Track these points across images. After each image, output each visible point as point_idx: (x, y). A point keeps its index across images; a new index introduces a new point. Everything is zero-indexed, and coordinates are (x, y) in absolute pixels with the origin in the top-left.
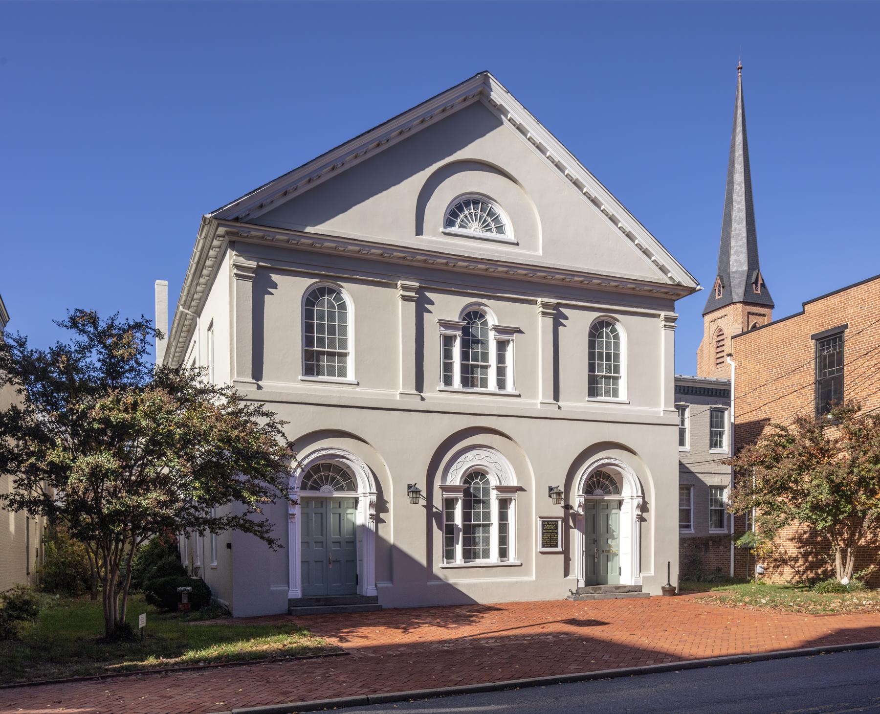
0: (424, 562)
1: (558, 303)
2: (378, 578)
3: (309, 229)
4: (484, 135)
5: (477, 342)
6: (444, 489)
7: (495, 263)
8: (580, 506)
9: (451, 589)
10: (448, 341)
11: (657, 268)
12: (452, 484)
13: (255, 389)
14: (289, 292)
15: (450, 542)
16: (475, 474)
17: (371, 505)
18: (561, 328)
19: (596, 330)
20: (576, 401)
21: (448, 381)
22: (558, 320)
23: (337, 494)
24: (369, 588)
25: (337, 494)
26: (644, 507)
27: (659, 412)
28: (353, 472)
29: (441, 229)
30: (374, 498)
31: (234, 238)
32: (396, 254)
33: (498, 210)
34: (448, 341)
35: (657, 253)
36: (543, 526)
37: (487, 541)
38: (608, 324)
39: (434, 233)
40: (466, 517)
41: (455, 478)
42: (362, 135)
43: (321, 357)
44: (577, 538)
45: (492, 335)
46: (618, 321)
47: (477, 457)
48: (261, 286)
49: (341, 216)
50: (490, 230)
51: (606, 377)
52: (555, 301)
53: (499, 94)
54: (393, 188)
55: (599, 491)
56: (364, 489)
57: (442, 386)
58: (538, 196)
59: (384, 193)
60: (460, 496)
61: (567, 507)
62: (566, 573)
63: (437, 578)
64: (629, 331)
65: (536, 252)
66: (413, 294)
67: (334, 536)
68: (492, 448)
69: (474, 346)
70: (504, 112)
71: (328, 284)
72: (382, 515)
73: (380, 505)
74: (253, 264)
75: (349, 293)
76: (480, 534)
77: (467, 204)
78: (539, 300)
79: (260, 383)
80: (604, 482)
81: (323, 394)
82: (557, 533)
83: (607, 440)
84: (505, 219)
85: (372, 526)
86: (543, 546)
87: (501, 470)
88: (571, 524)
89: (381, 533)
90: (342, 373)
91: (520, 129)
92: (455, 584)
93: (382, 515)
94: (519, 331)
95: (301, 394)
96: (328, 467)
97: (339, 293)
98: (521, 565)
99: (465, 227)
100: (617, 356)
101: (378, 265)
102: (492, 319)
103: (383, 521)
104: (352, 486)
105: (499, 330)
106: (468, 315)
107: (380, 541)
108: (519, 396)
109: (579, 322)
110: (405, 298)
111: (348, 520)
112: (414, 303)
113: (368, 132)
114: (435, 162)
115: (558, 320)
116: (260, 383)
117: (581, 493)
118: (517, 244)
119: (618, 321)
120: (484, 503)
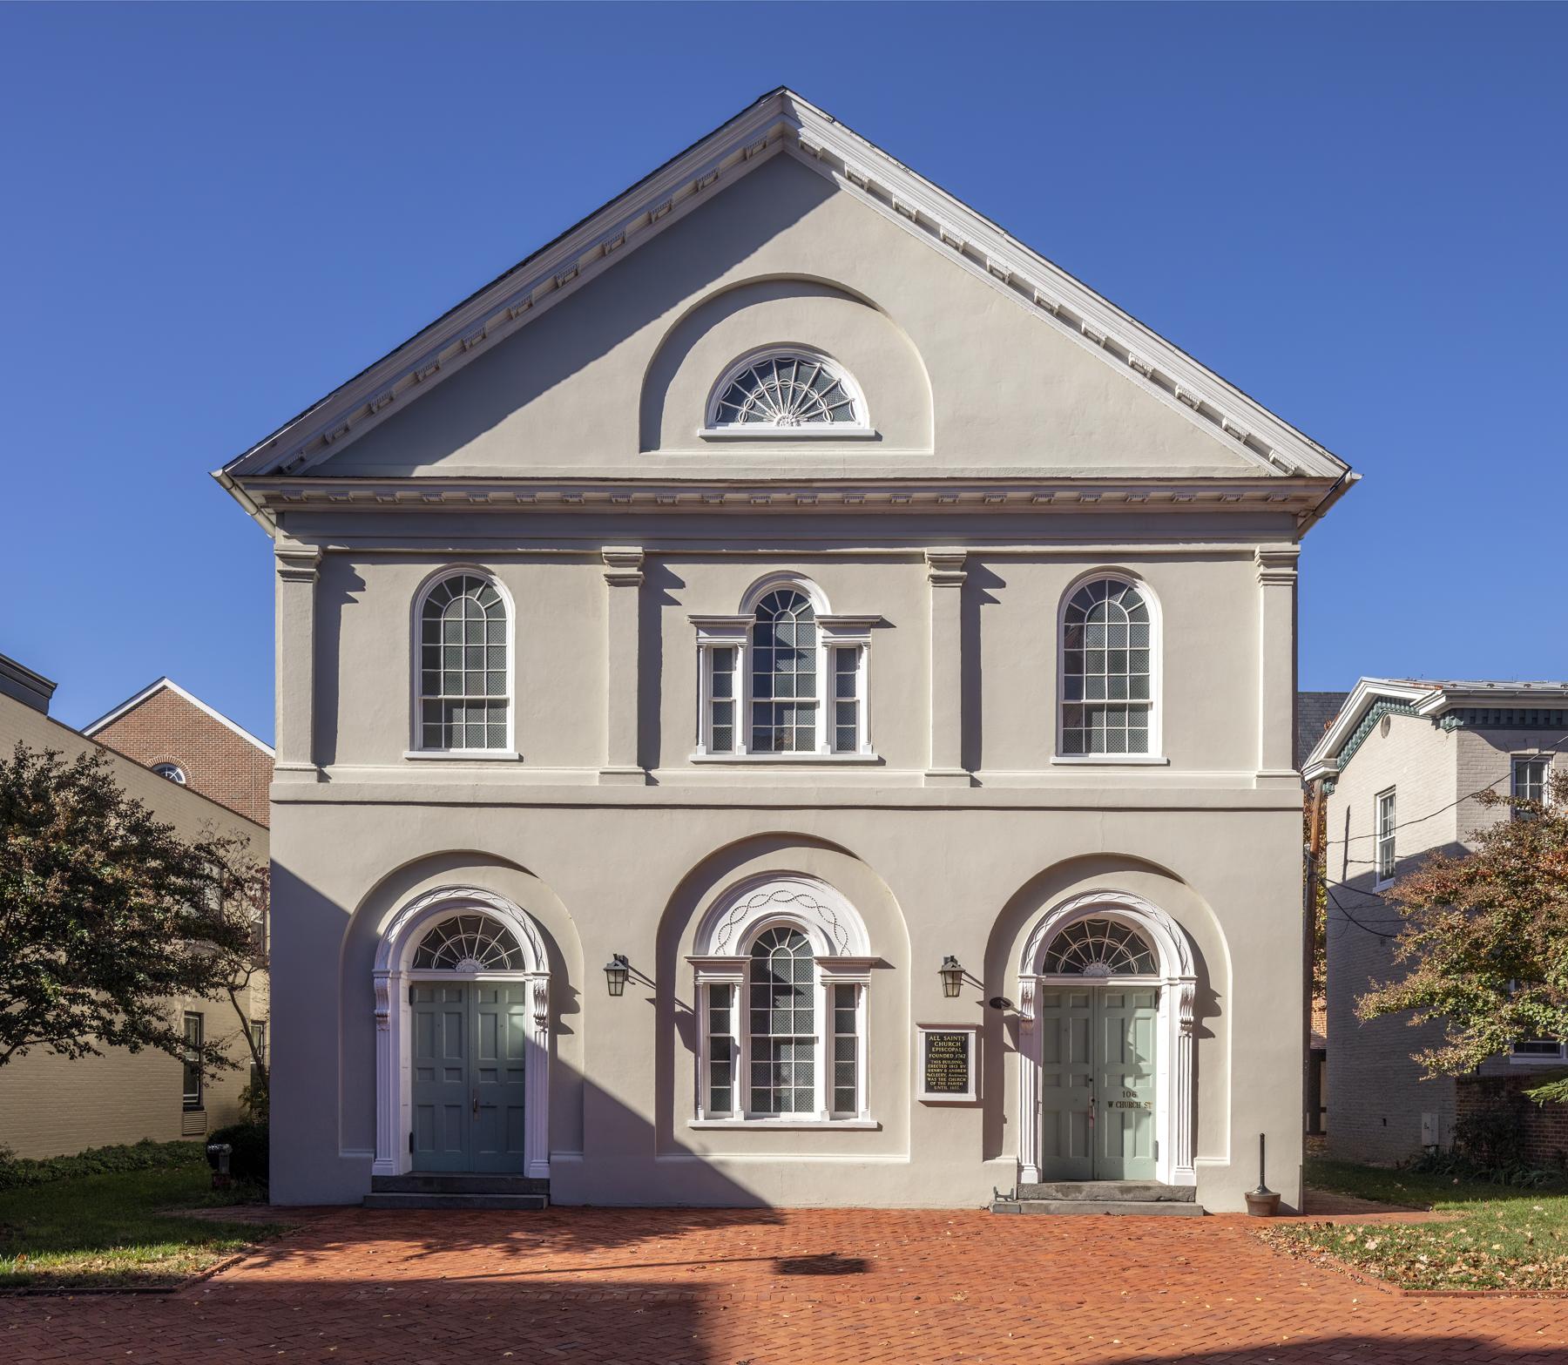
0: (650, 1115)
1: (969, 554)
2: (553, 1144)
3: (421, 471)
4: (796, 221)
5: (787, 654)
6: (699, 964)
7: (807, 485)
8: (1025, 1000)
9: (712, 1174)
10: (721, 659)
11: (1239, 445)
12: (720, 954)
13: (315, 782)
14: (388, 595)
15: (721, 1074)
16: (776, 935)
17: (1185, 1001)
18: (985, 609)
19: (1079, 609)
20: (1025, 761)
21: (721, 740)
22: (975, 589)
23: (1114, 982)
24: (536, 1167)
25: (1114, 982)
26: (1203, 1003)
27: (1248, 781)
28: (1150, 937)
29: (701, 430)
30: (1191, 988)
31: (282, 507)
32: (1154, 494)
33: (835, 371)
34: (721, 659)
35: (1230, 409)
36: (930, 1045)
37: (807, 1074)
38: (1116, 588)
39: (686, 441)
40: (758, 1022)
41: (727, 941)
42: (511, 271)
43: (456, 711)
44: (1022, 1076)
45: (820, 633)
46: (1140, 577)
47: (779, 897)
48: (332, 587)
49: (484, 435)
50: (818, 417)
51: (1112, 708)
52: (962, 550)
53: (817, 130)
54: (592, 365)
55: (1098, 966)
56: (1172, 965)
57: (701, 753)
58: (936, 328)
59: (574, 377)
60: (738, 978)
61: (996, 1003)
62: (992, 1145)
63: (685, 1150)
64: (1170, 599)
65: (920, 450)
66: (633, 571)
67: (482, 1057)
68: (813, 877)
69: (782, 664)
70: (837, 164)
71: (465, 570)
72: (1207, 1022)
73: (560, 997)
74: (313, 550)
75: (507, 582)
76: (790, 1058)
77: (764, 370)
78: (1258, 548)
79: (975, 774)
80: (1096, 951)
81: (444, 783)
82: (965, 1061)
83: (477, 848)
84: (852, 389)
85: (543, 1040)
86: (930, 1088)
87: (832, 918)
88: (1008, 1039)
89: (562, 1053)
90: (1139, 742)
91: (872, 190)
92: (722, 1163)
93: (1207, 1022)
94: (882, 623)
95: (398, 786)
96: (1099, 928)
97: (490, 586)
98: (880, 1128)
99: (760, 419)
100: (1141, 658)
101: (558, 522)
102: (821, 604)
103: (1209, 1034)
104: (1149, 965)
105: (835, 625)
106: (769, 600)
107: (560, 1070)
108: (881, 762)
109: (1032, 594)
110: (614, 581)
111: (513, 1026)
112: (635, 590)
113: (524, 264)
114: (684, 297)
115: (975, 589)
116: (975, 774)
117: (1029, 971)
118: (877, 437)
119: (1140, 577)
120: (798, 993)
